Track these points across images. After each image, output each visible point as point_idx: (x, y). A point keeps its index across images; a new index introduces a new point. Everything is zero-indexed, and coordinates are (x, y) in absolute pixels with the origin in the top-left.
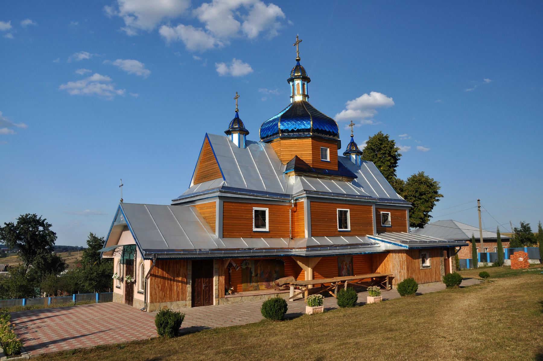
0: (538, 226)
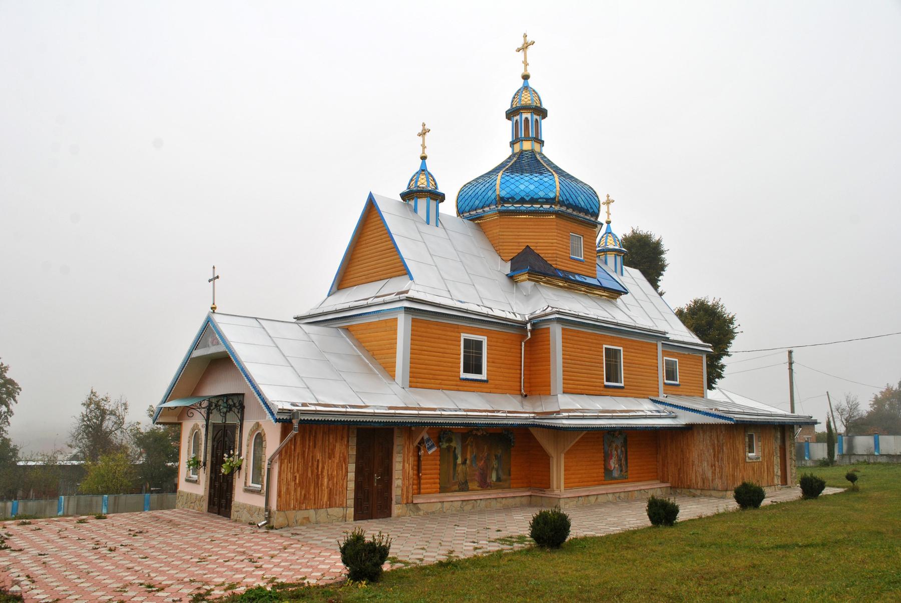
0: (873, 396)
